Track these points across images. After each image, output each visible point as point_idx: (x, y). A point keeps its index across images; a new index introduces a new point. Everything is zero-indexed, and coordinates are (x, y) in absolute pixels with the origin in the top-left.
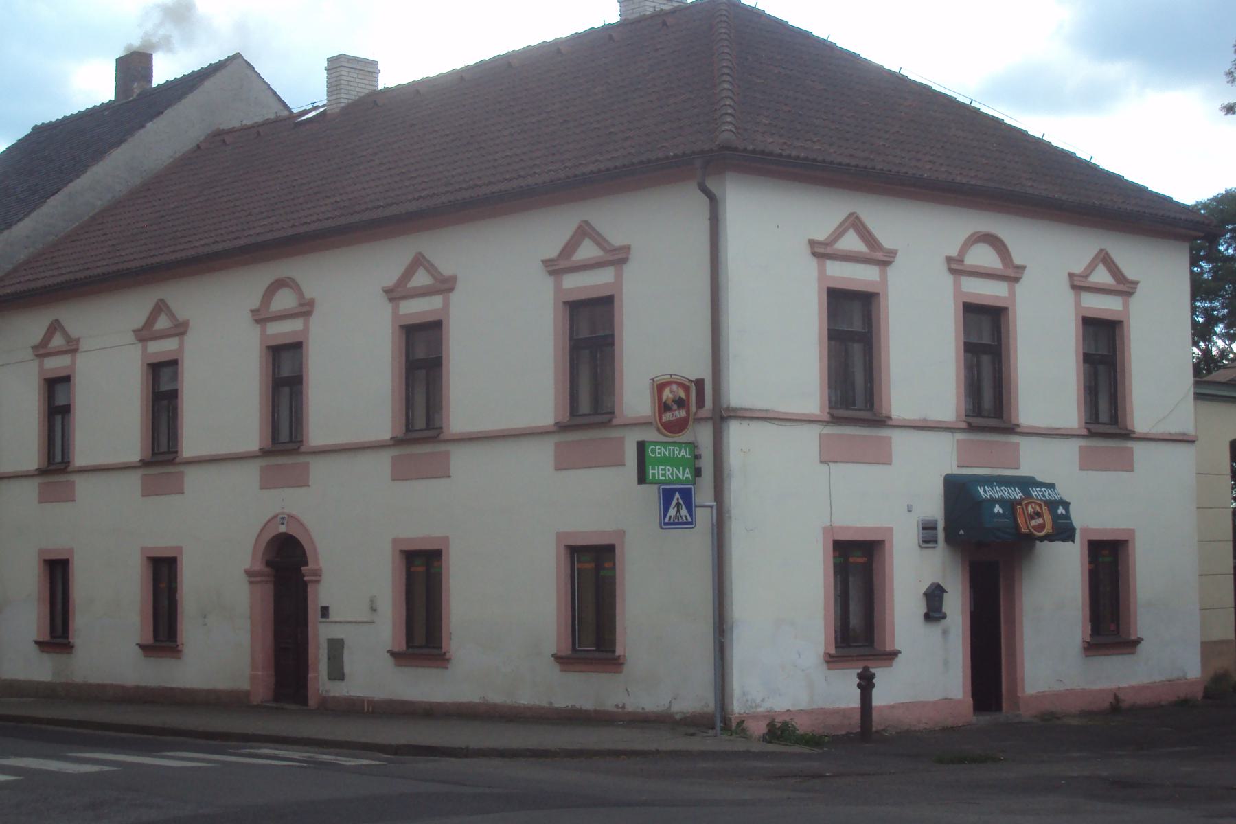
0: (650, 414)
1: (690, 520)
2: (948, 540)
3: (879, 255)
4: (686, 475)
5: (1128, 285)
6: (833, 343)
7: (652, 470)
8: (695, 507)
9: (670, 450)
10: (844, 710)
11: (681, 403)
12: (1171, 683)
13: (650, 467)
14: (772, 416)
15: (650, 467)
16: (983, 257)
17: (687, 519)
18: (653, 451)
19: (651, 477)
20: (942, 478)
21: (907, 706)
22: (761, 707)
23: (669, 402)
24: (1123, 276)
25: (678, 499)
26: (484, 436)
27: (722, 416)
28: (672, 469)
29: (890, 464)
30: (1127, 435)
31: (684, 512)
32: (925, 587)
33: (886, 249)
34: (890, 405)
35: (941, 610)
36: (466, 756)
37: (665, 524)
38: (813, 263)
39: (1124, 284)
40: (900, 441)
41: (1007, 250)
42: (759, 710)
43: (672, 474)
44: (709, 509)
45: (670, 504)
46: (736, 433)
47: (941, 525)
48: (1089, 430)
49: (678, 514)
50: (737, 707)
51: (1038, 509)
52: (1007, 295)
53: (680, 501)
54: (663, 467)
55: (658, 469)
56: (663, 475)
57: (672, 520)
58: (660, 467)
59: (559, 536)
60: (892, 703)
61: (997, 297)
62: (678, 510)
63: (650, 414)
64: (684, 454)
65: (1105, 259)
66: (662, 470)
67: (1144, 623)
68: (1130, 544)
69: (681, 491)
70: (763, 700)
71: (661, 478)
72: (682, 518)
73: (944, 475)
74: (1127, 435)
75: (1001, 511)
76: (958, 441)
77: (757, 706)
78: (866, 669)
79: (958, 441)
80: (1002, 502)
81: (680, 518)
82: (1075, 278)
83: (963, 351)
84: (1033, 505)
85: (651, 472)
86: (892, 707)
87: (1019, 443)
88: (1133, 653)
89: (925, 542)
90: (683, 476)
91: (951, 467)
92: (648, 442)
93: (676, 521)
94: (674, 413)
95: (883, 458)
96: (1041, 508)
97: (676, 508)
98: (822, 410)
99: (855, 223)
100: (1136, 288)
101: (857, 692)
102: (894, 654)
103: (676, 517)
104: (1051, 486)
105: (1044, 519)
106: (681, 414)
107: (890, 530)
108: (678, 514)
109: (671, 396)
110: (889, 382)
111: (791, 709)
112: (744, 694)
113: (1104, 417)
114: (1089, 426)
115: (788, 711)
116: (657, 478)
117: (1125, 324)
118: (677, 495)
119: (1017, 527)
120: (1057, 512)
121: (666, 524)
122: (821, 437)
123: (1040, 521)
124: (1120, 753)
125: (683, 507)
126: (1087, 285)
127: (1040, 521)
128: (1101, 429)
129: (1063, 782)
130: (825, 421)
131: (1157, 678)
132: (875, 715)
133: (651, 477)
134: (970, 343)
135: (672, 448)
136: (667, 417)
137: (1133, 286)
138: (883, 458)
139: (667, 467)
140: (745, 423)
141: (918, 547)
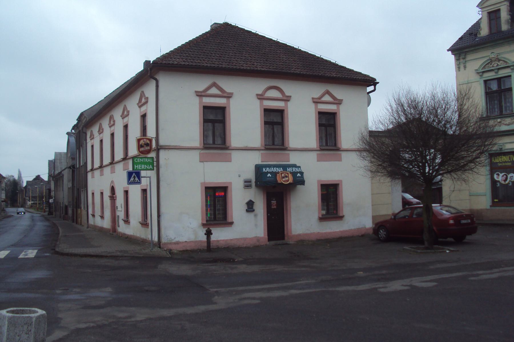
1: (139, 182)
2: (257, 185)
3: (225, 95)
4: (150, 167)
5: (338, 101)
6: (267, 126)
7: (136, 166)
9: (143, 160)
11: (147, 145)
12: (358, 229)
13: (135, 165)
14: (178, 148)
15: (135, 165)
16: (327, 98)
17: (138, 181)
18: (137, 160)
19: (135, 168)
20: (254, 165)
21: (238, 239)
22: (174, 240)
23: (143, 145)
24: (336, 98)
25: (134, 175)
27: (158, 149)
28: (145, 166)
30: (338, 150)
31: (137, 179)
32: (247, 200)
33: (227, 92)
35: (253, 208)
39: (337, 101)
40: (235, 155)
41: (281, 90)
42: (173, 241)
44: (149, 178)
45: (131, 176)
46: (162, 153)
47: (254, 180)
48: (320, 148)
50: (164, 240)
51: (287, 175)
52: (336, 109)
53: (135, 176)
54: (141, 165)
55: (139, 166)
56: (140, 168)
57: (132, 182)
60: (232, 238)
62: (134, 179)
64: (150, 161)
65: (328, 93)
66: (140, 166)
67: (346, 210)
68: (340, 186)
70: (175, 238)
71: (140, 168)
72: (136, 181)
74: (338, 150)
75: (270, 176)
76: (261, 153)
77: (172, 240)
78: (209, 228)
79: (261, 153)
80: (270, 173)
82: (314, 99)
83: (318, 126)
84: (285, 174)
85: (135, 167)
86: (231, 240)
89: (245, 186)
90: (149, 168)
91: (259, 162)
94: (145, 148)
95: (340, 160)
98: (200, 144)
99: (328, 93)
100: (342, 102)
101: (205, 236)
102: (231, 223)
103: (133, 181)
104: (300, 167)
105: (289, 178)
107: (231, 183)
109: (143, 143)
110: (230, 136)
111: (187, 241)
113: (324, 144)
116: (138, 168)
117: (338, 114)
118: (134, 174)
119: (277, 181)
120: (297, 175)
121: (129, 183)
122: (200, 154)
123: (287, 179)
124: (105, 270)
125: (136, 177)
127: (287, 179)
128: (324, 148)
130: (201, 149)
131: (353, 228)
133: (135, 168)
134: (320, 124)
135: (144, 159)
137: (340, 101)
138: (340, 160)
139: (142, 165)
140: (167, 151)
141: (244, 189)
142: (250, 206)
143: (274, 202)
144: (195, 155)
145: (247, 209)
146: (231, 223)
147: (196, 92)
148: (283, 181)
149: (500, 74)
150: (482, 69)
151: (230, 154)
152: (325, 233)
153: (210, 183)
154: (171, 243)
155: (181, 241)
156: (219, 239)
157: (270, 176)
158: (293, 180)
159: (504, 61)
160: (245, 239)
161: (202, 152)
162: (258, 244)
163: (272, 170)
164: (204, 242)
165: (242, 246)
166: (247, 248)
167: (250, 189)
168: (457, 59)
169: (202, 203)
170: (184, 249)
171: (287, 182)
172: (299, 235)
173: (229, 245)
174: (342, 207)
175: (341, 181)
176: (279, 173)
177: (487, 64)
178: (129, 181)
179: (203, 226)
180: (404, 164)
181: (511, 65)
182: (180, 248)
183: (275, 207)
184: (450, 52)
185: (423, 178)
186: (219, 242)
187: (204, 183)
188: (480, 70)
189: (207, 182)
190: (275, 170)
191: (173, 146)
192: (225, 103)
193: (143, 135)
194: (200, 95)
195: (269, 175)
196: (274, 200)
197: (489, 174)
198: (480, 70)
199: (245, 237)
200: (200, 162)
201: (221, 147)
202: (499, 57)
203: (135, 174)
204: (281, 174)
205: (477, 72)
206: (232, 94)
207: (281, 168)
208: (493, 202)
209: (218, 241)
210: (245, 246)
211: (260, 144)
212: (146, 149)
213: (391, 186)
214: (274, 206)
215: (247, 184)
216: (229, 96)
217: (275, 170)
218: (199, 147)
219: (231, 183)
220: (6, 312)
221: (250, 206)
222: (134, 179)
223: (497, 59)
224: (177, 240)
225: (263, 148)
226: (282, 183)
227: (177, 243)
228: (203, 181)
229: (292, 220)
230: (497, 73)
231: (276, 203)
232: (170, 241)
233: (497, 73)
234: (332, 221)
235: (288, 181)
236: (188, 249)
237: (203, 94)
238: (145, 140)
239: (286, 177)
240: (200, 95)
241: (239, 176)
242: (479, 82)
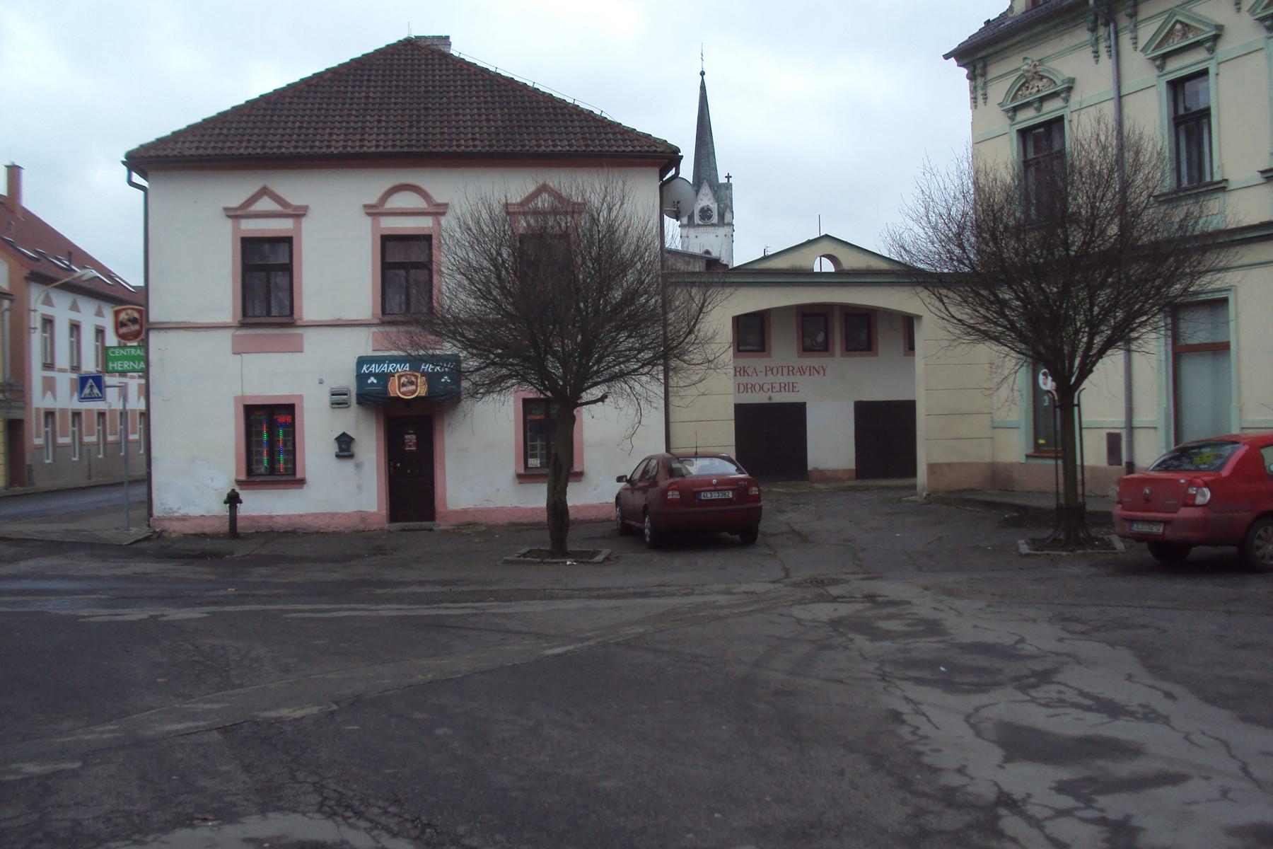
0: (305, 320)
1: (100, 395)
2: (359, 403)
3: (290, 211)
4: (141, 366)
10: (253, 517)
18: (113, 353)
21: (316, 515)
23: (125, 321)
29: (302, 352)
31: (96, 391)
38: (369, 220)
40: (310, 336)
42: (176, 514)
43: (129, 366)
46: (155, 339)
51: (414, 379)
53: (93, 384)
56: (121, 367)
58: (119, 362)
60: (302, 513)
61: (423, 228)
62: (92, 390)
63: (305, 320)
69: (93, 378)
70: (179, 509)
73: (357, 357)
75: (375, 381)
76: (373, 332)
80: (376, 375)
86: (302, 516)
87: (1227, 297)
88: (580, 481)
96: (417, 379)
98: (234, 316)
103: (90, 394)
106: (136, 327)
107: (301, 397)
109: (126, 317)
112: (162, 504)
114: (293, 321)
115: (202, 516)
118: (91, 381)
121: (82, 398)
122: (234, 337)
126: (383, 211)
129: (898, 535)
132: (240, 524)
135: (129, 350)
136: (123, 330)
140: (162, 332)
142: (343, 446)
143: (411, 438)
144: (225, 338)
145: (337, 450)
146: (301, 482)
147: (226, 209)
148: (402, 393)
149: (1045, 114)
150: (1012, 101)
151: (301, 336)
152: (532, 509)
153: (252, 397)
154: (170, 519)
155: (192, 514)
156: (274, 514)
157: (375, 381)
158: (430, 390)
159: (1051, 79)
160: (333, 515)
161: (382, 329)
162: (362, 526)
163: (383, 369)
164: (221, 517)
165: (326, 531)
166: (336, 534)
167: (346, 409)
168: (972, 77)
169: (237, 439)
170: (198, 530)
171: (412, 395)
172: (465, 511)
173: (296, 526)
174: (582, 450)
176: (394, 376)
177: (1019, 89)
179: (239, 485)
180: (554, 354)
181: (1061, 87)
182: (189, 528)
183: (414, 448)
184: (952, 60)
186: (274, 520)
187: (242, 397)
188: (1008, 103)
189: (248, 394)
190: (390, 368)
191: (176, 323)
192: (290, 229)
194: (234, 215)
195: (372, 380)
196: (411, 434)
198: (1008, 103)
199: (333, 510)
200: (234, 353)
201: (1220, 293)
202: (1039, 69)
203: (93, 380)
204: (400, 377)
205: (1003, 109)
206: (306, 208)
207: (408, 365)
208: (1037, 445)
209: (271, 517)
210: (331, 529)
211: (371, 313)
212: (133, 329)
214: (410, 446)
215: (338, 400)
216: (299, 214)
217: (385, 368)
218: (230, 323)
219: (301, 397)
221: (345, 446)
222: (92, 390)
223: (1036, 73)
224: (184, 511)
225: (376, 321)
226: (399, 397)
227: (184, 518)
228: (240, 394)
229: (448, 479)
230: (1038, 110)
231: (417, 439)
232: (170, 513)
233: (1038, 110)
234: (539, 482)
235: (415, 392)
236: (207, 530)
237: (239, 213)
238: (129, 311)
239: (412, 383)
240: (234, 215)
241: (321, 382)
242: (1007, 135)
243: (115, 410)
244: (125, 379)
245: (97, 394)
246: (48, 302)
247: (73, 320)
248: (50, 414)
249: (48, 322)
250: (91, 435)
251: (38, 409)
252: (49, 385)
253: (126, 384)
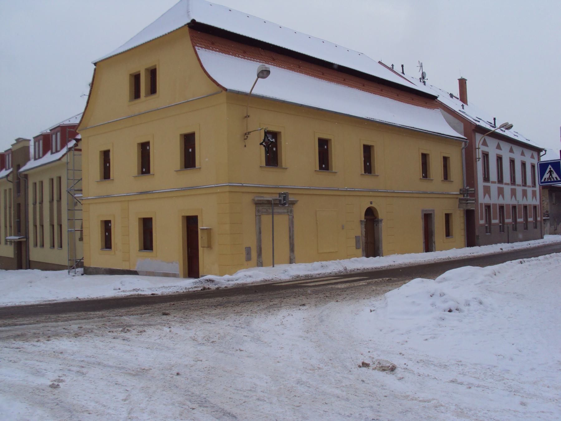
8: (354, 238)
25: (550, 168)
26: (147, 112)
34: (130, 79)
36: (155, 303)
37: (542, 183)
49: (551, 177)
53: (552, 169)
57: (546, 181)
59: (423, 211)
62: (551, 175)
72: (553, 179)
81: (552, 179)
92: (290, 194)
93: (549, 180)
97: (549, 174)
103: (549, 178)
108: (551, 177)
118: (550, 166)
125: (554, 172)
175: (423, 211)
178: (541, 179)
185: (109, 224)
193: (206, 246)
197: (463, 229)
213: (221, 319)
220: (253, 200)
222: (551, 175)
243: (521, 205)
244: (502, 185)
245: (556, 178)
246: (485, 144)
247: (484, 151)
248: (488, 207)
249: (486, 155)
250: (509, 218)
251: (481, 204)
252: (487, 190)
253: (503, 188)
